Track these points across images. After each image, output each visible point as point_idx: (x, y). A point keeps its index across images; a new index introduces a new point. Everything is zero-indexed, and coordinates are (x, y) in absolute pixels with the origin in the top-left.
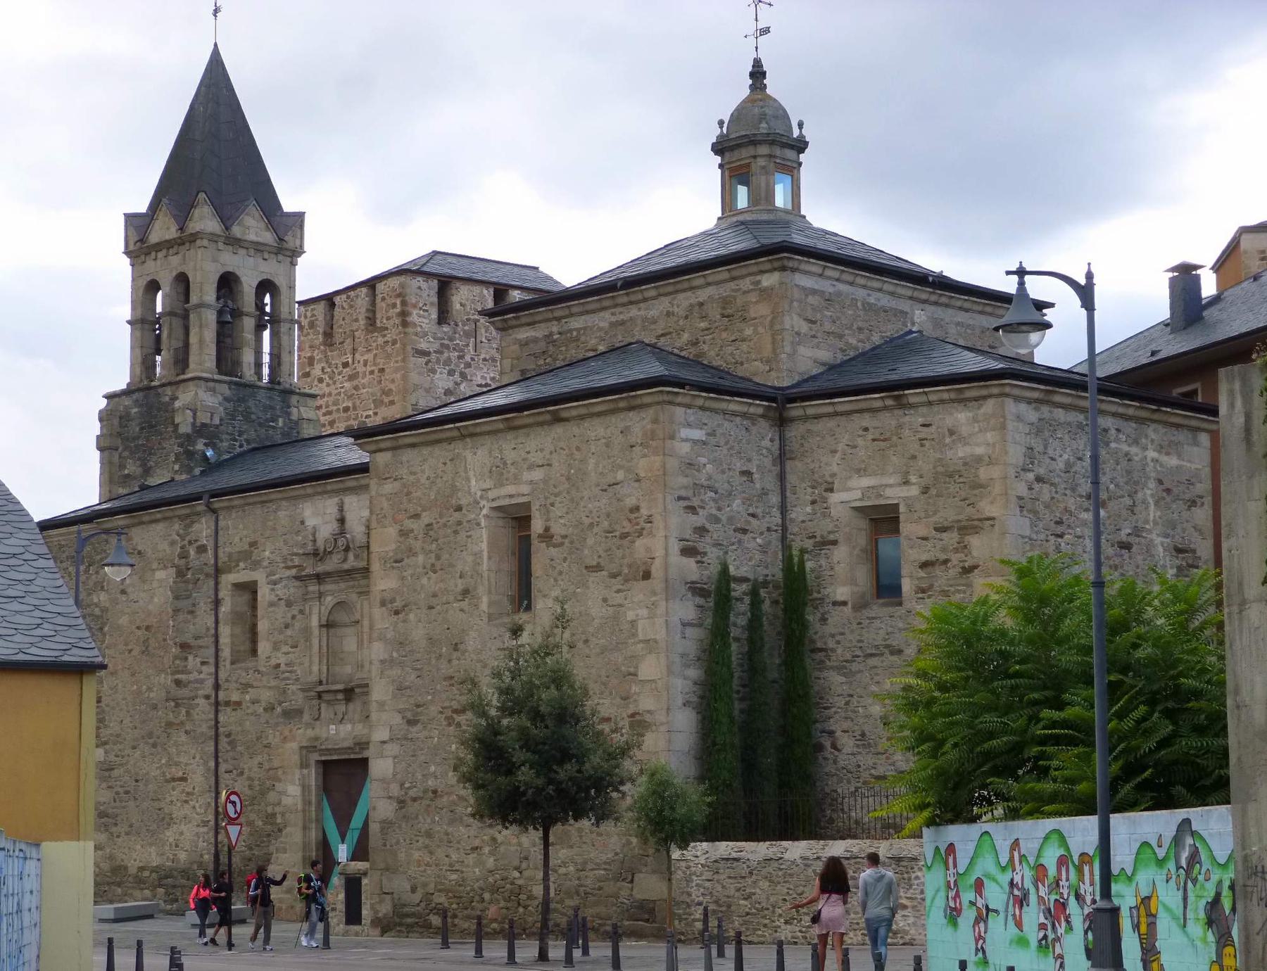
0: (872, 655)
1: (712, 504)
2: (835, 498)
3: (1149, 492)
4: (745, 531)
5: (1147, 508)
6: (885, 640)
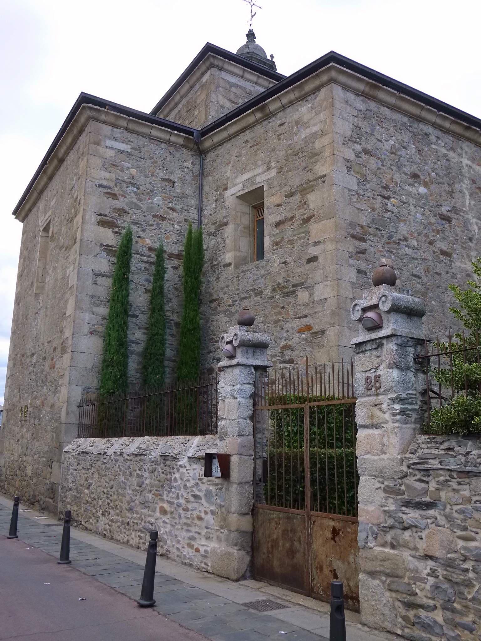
0: (244, 298)
1: (133, 195)
2: (228, 193)
3: (465, 186)
4: (163, 218)
5: (463, 196)
6: (252, 285)
